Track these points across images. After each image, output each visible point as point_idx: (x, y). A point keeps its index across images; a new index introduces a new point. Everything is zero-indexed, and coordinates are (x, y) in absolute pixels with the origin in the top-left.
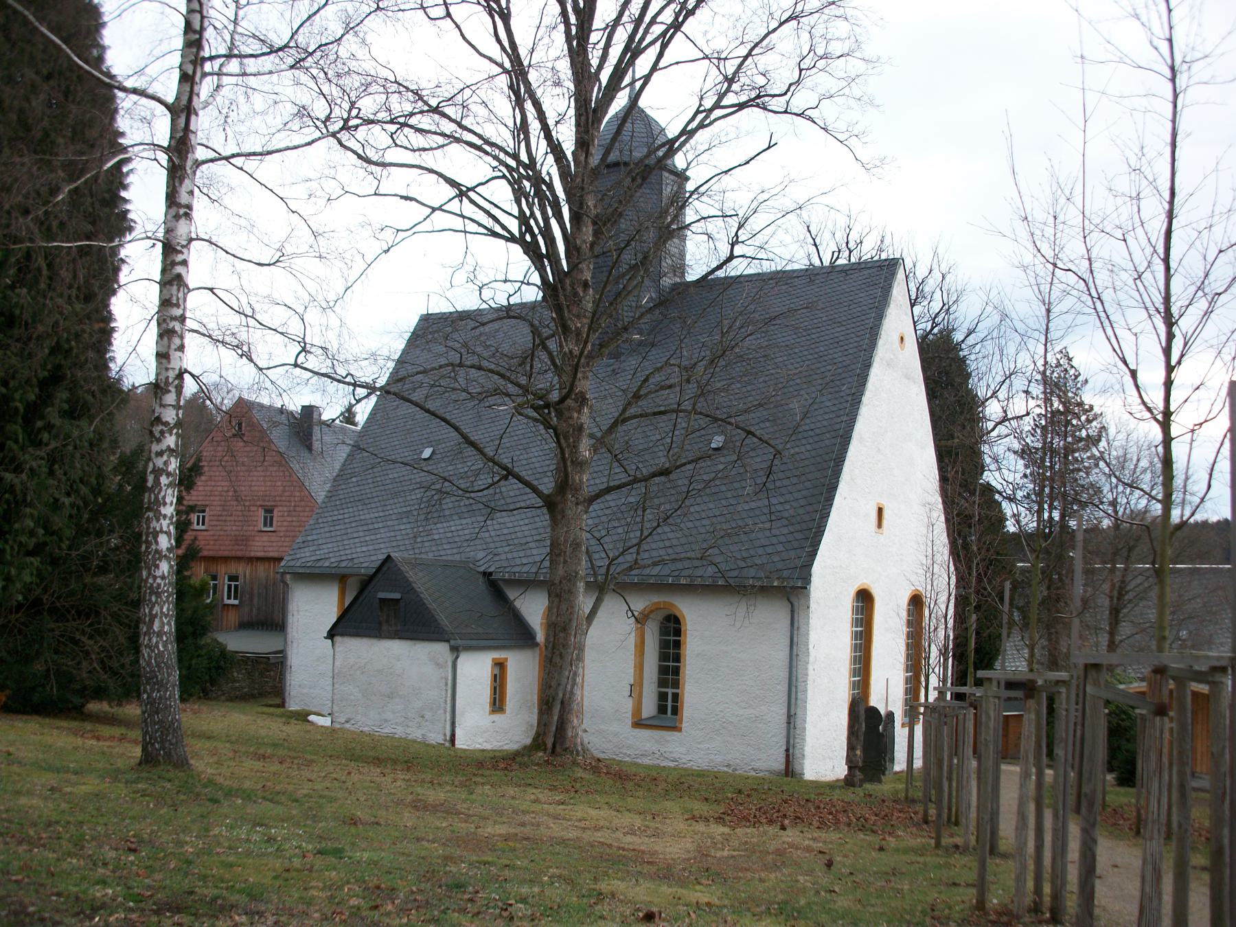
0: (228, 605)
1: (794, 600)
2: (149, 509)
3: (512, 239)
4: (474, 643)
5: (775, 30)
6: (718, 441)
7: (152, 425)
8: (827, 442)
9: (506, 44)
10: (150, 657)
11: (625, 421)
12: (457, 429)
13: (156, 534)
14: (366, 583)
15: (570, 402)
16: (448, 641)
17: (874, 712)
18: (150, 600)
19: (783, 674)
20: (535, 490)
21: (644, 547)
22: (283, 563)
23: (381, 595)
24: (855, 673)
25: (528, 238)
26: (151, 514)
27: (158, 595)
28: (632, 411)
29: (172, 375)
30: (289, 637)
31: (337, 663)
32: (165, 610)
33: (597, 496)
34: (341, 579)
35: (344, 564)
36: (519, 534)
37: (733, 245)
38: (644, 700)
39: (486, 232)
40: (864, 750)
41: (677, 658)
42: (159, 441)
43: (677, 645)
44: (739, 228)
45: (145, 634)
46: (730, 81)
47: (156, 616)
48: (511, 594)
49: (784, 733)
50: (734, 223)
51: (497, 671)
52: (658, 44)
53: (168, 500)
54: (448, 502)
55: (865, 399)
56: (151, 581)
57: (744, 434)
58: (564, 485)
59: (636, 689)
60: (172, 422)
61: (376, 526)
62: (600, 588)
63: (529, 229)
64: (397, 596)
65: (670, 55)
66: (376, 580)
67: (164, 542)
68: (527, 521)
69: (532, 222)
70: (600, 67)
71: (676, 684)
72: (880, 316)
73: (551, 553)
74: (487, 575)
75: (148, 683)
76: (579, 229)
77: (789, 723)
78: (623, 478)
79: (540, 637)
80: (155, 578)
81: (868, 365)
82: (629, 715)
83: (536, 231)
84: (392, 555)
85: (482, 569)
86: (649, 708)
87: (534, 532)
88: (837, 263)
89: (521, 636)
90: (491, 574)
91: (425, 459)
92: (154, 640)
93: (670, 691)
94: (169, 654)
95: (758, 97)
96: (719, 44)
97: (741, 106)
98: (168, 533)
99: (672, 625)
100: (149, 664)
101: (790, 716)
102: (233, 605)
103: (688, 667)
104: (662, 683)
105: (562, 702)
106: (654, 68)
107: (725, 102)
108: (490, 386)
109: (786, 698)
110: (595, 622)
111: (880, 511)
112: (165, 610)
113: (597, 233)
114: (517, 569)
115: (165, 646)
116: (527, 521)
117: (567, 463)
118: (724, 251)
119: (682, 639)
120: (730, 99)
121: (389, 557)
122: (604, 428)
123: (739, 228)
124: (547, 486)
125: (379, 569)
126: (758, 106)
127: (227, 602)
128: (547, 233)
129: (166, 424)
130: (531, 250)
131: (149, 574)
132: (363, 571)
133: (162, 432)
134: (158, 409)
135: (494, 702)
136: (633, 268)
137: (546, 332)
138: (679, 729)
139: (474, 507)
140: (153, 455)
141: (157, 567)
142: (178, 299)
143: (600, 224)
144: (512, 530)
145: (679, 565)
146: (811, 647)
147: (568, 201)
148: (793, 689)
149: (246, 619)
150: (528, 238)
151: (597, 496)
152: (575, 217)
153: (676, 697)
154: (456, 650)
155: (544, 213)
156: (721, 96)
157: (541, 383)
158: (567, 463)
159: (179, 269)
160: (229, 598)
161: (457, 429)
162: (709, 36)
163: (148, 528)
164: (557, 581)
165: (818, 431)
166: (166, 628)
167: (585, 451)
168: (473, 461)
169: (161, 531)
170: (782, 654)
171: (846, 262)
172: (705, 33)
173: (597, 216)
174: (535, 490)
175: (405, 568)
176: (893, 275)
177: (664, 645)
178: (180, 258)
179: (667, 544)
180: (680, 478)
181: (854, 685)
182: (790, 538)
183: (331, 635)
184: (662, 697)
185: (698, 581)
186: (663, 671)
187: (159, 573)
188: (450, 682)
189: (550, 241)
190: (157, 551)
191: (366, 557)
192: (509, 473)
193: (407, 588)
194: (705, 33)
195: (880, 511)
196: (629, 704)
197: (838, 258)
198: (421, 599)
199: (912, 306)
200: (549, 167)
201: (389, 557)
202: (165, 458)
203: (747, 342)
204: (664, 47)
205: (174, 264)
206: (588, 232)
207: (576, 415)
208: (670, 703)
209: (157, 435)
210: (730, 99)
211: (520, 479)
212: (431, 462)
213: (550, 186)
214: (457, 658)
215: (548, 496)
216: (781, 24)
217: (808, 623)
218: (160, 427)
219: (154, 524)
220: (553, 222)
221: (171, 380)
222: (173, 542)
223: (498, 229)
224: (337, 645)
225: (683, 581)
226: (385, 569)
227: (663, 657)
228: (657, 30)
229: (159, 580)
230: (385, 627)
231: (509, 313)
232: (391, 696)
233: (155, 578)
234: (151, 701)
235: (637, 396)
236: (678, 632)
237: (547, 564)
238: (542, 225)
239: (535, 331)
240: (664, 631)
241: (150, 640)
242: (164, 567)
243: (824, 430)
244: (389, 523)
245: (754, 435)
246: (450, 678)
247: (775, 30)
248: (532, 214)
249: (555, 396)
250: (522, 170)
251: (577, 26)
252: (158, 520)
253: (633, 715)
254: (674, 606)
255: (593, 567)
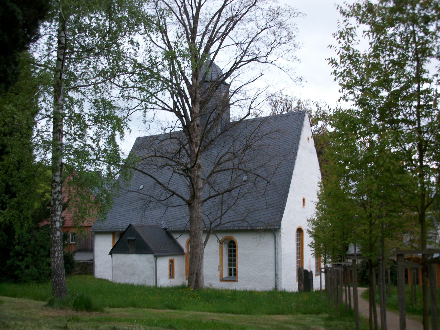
0: (72, 244)
1: (275, 233)
2: (52, 213)
3: (171, 110)
4: (168, 254)
5: (260, 33)
6: (245, 178)
7: (52, 183)
8: (284, 177)
9: (166, 42)
10: (54, 266)
11: (214, 173)
12: (154, 179)
13: (55, 222)
14: (122, 234)
15: (195, 168)
16: (153, 254)
17: (306, 271)
18: (54, 245)
19: (273, 260)
20: (183, 199)
21: (222, 217)
22: (92, 228)
23: (128, 238)
24: (298, 258)
25: (177, 110)
26: (53, 215)
27: (57, 243)
28: (217, 169)
29: (58, 165)
30: (95, 254)
31: (114, 263)
32: (59, 248)
33: (206, 200)
34: (113, 233)
35: (114, 228)
36: (176, 214)
37: (249, 109)
38: (224, 272)
39: (161, 108)
40: (304, 285)
41: (235, 256)
42: (55, 188)
43: (235, 251)
44: (251, 104)
45: (53, 257)
46: (245, 52)
47: (56, 251)
48: (175, 236)
49: (274, 281)
50: (249, 101)
51: (171, 264)
52: (220, 41)
53: (59, 209)
54: (152, 205)
55: (297, 161)
56: (54, 238)
57: (256, 176)
58: (194, 196)
59: (220, 268)
60: (59, 182)
61: (125, 213)
62: (209, 232)
63: (177, 107)
64: (134, 238)
65: (225, 43)
66: (126, 233)
67: (58, 225)
68: (178, 210)
69: (178, 104)
70: (200, 48)
71: (235, 265)
72: (300, 132)
73: (190, 220)
74: (165, 229)
75: (54, 275)
76: (195, 106)
77: (276, 277)
78: (215, 193)
79: (185, 251)
80: (55, 237)
81: (297, 149)
82: (219, 277)
83: (180, 107)
84: (132, 224)
85: (163, 227)
86: (226, 274)
87: (181, 213)
88: (283, 113)
89: (179, 251)
90: (167, 229)
91: (141, 189)
92: (56, 259)
93: (233, 268)
94: (62, 264)
95: (257, 57)
96: (240, 39)
97: (250, 61)
98: (59, 221)
99: (232, 244)
100: (54, 268)
101: (276, 275)
102: (73, 244)
103: (239, 259)
104: (230, 265)
105: (197, 274)
106: (219, 48)
107: (243, 60)
108: (164, 163)
109: (274, 268)
110: (207, 246)
111: (304, 200)
112: (59, 248)
113: (201, 108)
114: (176, 227)
115: (60, 261)
116: (178, 210)
117: (193, 188)
118: (246, 113)
119: (236, 249)
120: (246, 58)
121: (130, 225)
122: (207, 176)
123: (251, 104)
124: (187, 198)
125: (127, 229)
126: (256, 60)
127: (71, 243)
128: (184, 108)
129: (57, 182)
130: (178, 114)
131: (53, 236)
132: (121, 230)
133: (56, 185)
134: (54, 178)
135: (170, 275)
136: (214, 120)
137: (185, 143)
138: (237, 281)
139: (160, 205)
140: (53, 194)
141: (56, 233)
142: (59, 138)
143: (203, 104)
144: (173, 213)
145: (234, 223)
146: (282, 249)
147: (191, 96)
148: (277, 265)
149: (78, 249)
150: (177, 110)
151: (206, 200)
152: (193, 102)
153: (235, 270)
154: (156, 257)
155: (182, 100)
156: (242, 57)
157: (184, 160)
158: (193, 188)
159: (59, 127)
160: (72, 241)
161: (154, 179)
162: (237, 36)
163: (52, 219)
164: (193, 231)
165: (280, 173)
166: (60, 255)
167: (200, 184)
168: (160, 189)
169: (57, 221)
170: (272, 253)
171: (287, 113)
172: (235, 35)
173: (201, 101)
174: (183, 199)
175: (136, 228)
176: (304, 116)
177: (230, 251)
178: (60, 123)
179: (229, 215)
180: (234, 193)
181: (298, 262)
182: (273, 211)
183: (111, 253)
184: (230, 270)
185: (241, 228)
186: (230, 261)
187: (57, 236)
188: (154, 269)
189: (185, 111)
190: (55, 228)
191: (122, 225)
192: (174, 193)
193: (138, 235)
194: (235, 35)
195: (304, 200)
196: (218, 273)
197: (283, 111)
198: (143, 239)
199: (311, 126)
200: (183, 85)
201: (130, 225)
202: (57, 194)
203: (255, 144)
204: (222, 40)
205: (57, 126)
206: (198, 106)
207: (197, 172)
208: (233, 272)
209: (54, 186)
210: (246, 58)
211: (177, 195)
212: (143, 190)
213: (184, 91)
214: (156, 260)
215: (188, 201)
216: (262, 31)
217: (281, 241)
218: (55, 184)
219: (54, 218)
220: (186, 104)
221: (58, 166)
222: (61, 224)
223: (166, 107)
224: (113, 257)
225: (236, 228)
226: (129, 229)
227: (230, 256)
228: (219, 35)
229: (57, 238)
230: (130, 250)
231: (171, 136)
232: (133, 274)
233: (55, 237)
234: (55, 282)
235: (218, 164)
236: (235, 247)
237: (189, 224)
238: (182, 105)
239: (181, 143)
240: (230, 246)
241: (54, 259)
242: (58, 233)
243: (283, 172)
244: (129, 212)
245: (260, 177)
246: (154, 267)
247: (260, 33)
248: (178, 100)
249: (189, 166)
250: (173, 86)
251: (191, 34)
252: (55, 217)
253: (220, 277)
254: (232, 237)
255: (205, 224)
